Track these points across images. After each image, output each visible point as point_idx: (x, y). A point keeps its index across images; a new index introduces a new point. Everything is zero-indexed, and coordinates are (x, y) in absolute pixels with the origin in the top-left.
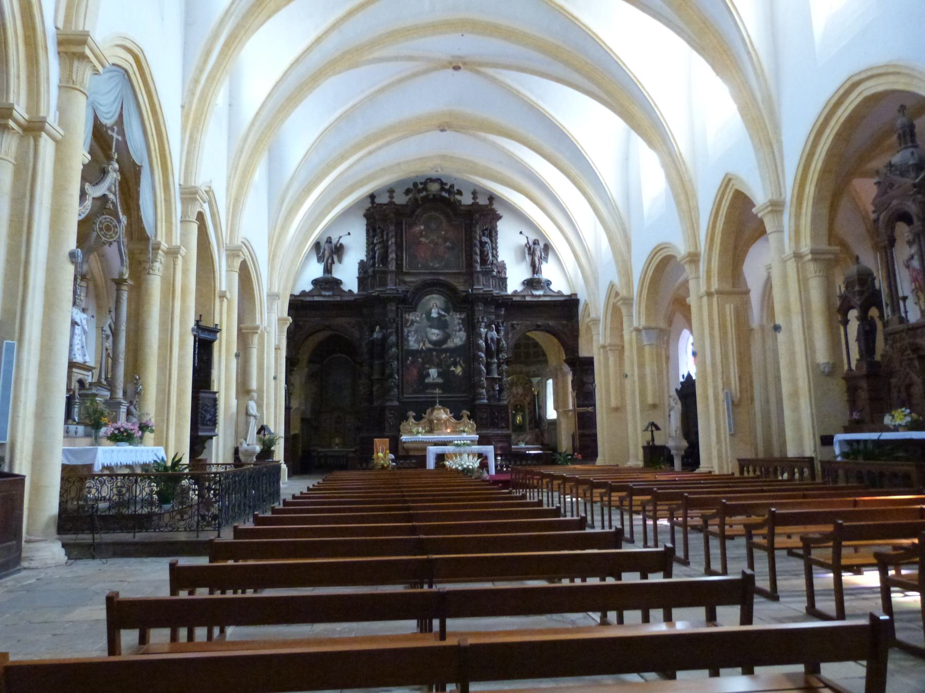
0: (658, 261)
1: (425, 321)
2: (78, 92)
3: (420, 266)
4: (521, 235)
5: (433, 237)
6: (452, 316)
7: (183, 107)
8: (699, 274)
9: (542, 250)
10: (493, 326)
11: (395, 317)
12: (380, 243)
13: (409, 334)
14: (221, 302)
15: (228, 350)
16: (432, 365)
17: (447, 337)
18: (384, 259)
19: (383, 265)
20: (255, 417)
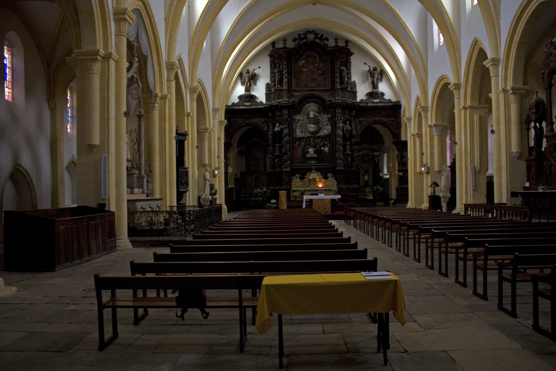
0: (441, 86)
1: (306, 120)
2: (123, 36)
3: (302, 85)
4: (365, 65)
5: (311, 67)
6: (322, 116)
7: (165, 19)
8: (460, 96)
9: (379, 74)
10: (348, 122)
11: (287, 117)
12: (278, 72)
13: (297, 128)
14: (188, 118)
15: (192, 143)
16: (311, 146)
18: (281, 82)
19: (280, 86)
20: (209, 180)
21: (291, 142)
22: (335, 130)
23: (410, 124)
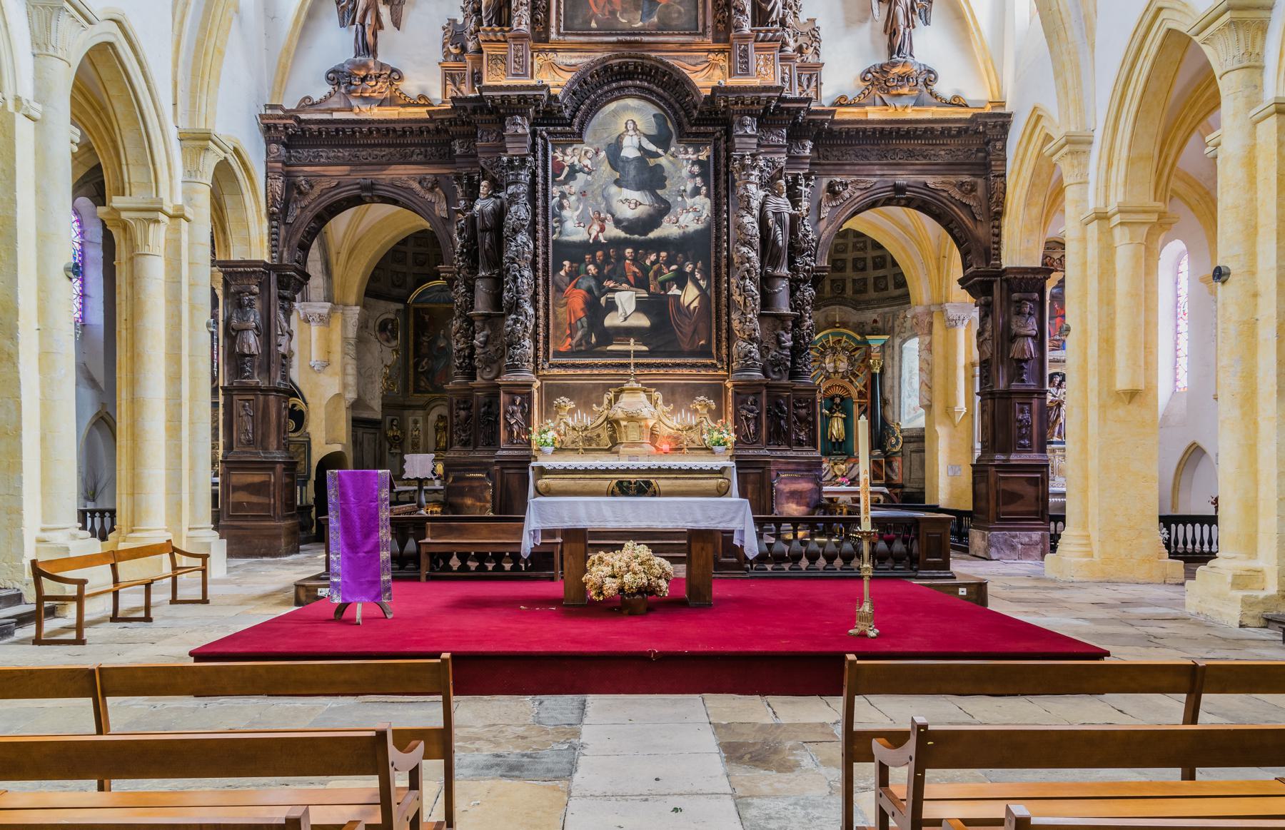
1: (605, 168)
3: (594, 25)
13: (565, 202)
17: (662, 210)
21: (540, 260)
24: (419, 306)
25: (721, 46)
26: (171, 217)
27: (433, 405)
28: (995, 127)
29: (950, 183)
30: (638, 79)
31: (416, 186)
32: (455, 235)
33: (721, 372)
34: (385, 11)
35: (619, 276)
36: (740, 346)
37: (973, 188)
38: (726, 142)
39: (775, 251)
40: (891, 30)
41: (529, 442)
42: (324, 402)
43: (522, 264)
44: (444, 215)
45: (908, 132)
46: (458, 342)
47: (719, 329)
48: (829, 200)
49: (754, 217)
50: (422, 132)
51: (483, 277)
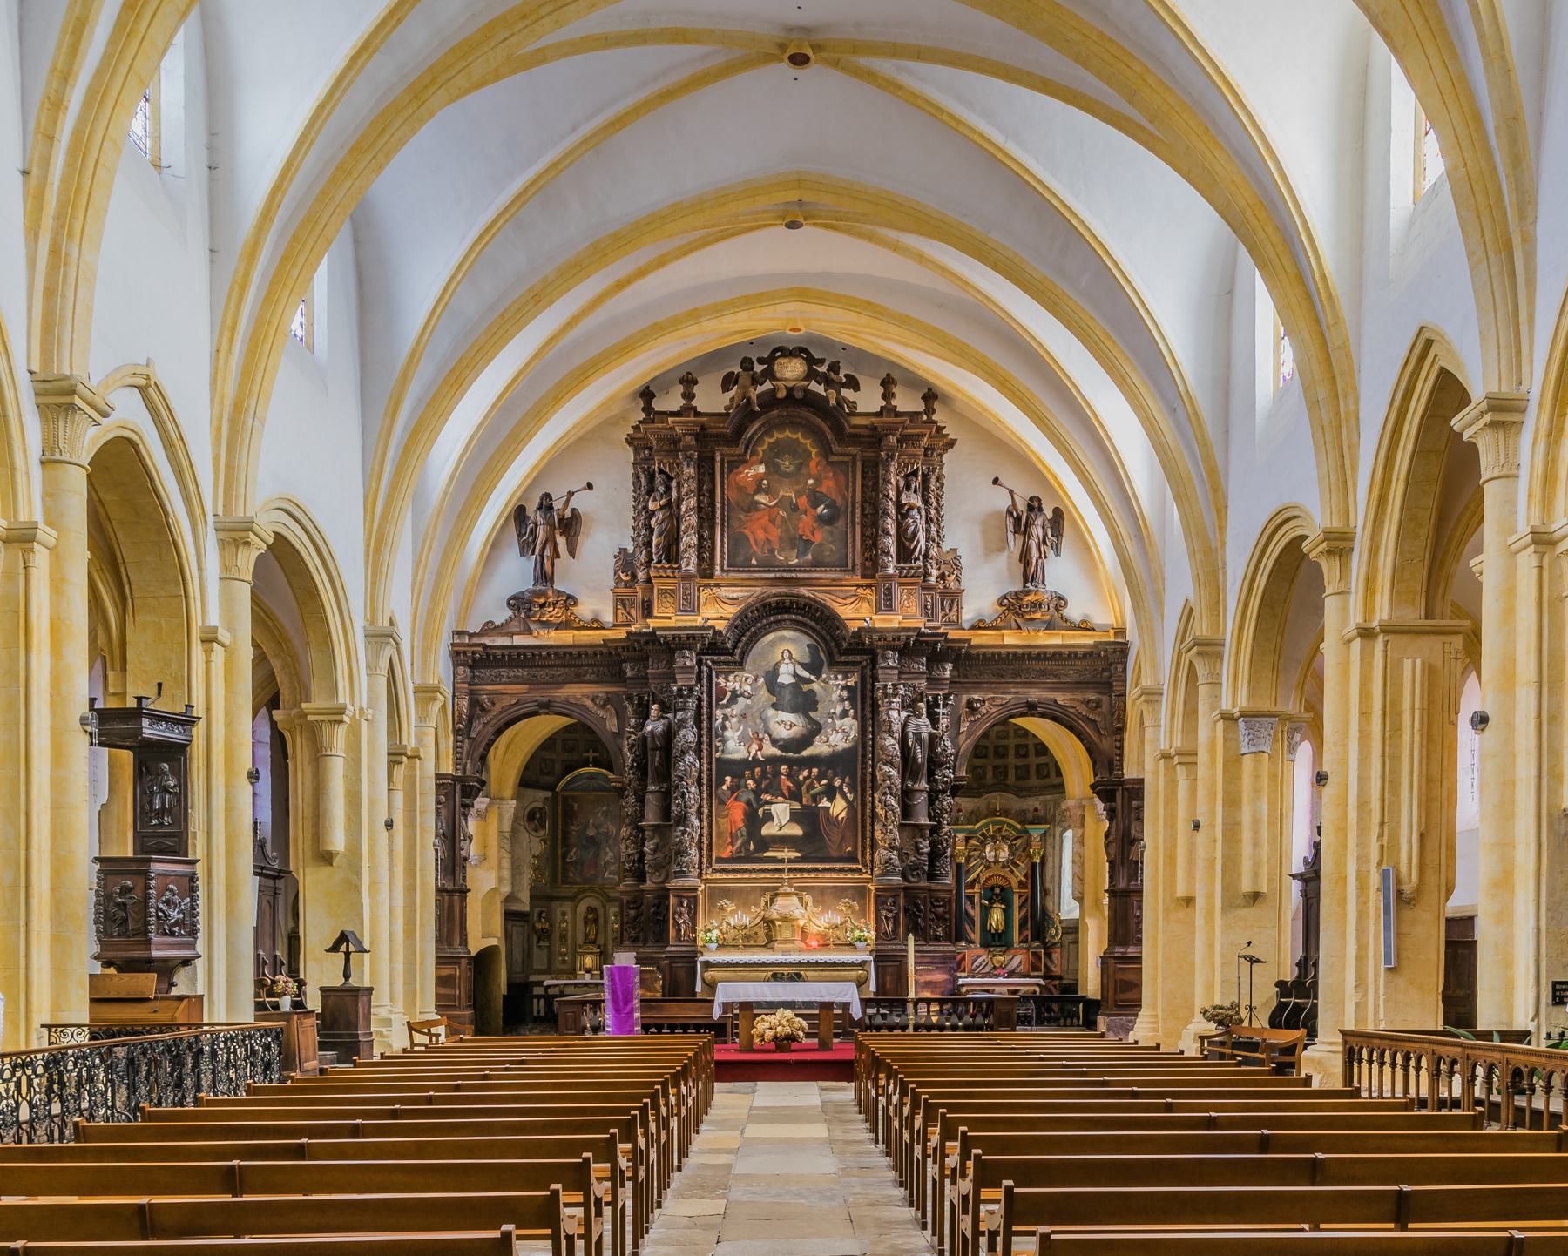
1: (764, 693)
3: (754, 562)
5: (787, 492)
8: (1348, 584)
10: (923, 705)
17: (815, 730)
21: (704, 776)
22: (873, 733)
23: (1157, 712)
24: (568, 794)
25: (869, 581)
26: (408, 758)
27: (581, 896)
28: (1115, 651)
29: (1078, 700)
30: (794, 613)
31: (589, 703)
32: (626, 750)
33: (865, 876)
34: (561, 541)
35: (775, 790)
36: (882, 853)
37: (1098, 704)
38: (871, 670)
39: (914, 767)
40: (1025, 558)
41: (695, 940)
42: (480, 897)
43: (689, 781)
44: (615, 729)
45: (1039, 654)
46: (627, 847)
47: (864, 837)
48: (968, 715)
49: (895, 739)
50: (595, 655)
51: (653, 792)
